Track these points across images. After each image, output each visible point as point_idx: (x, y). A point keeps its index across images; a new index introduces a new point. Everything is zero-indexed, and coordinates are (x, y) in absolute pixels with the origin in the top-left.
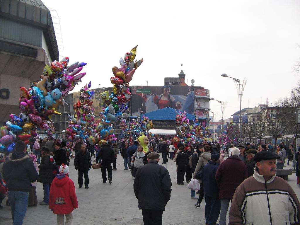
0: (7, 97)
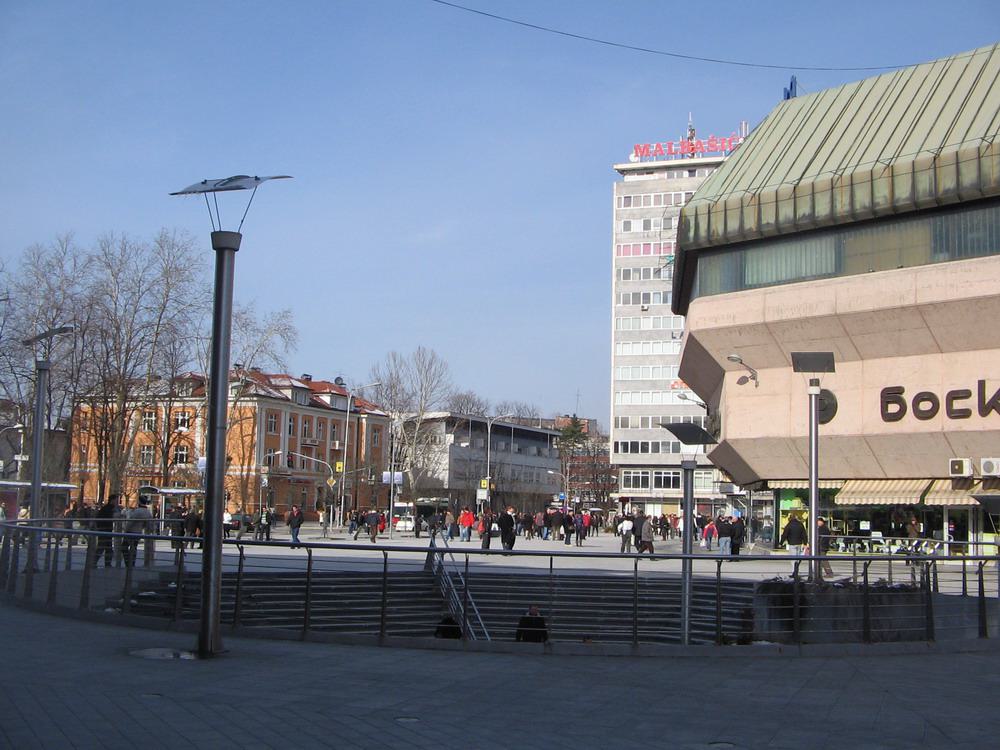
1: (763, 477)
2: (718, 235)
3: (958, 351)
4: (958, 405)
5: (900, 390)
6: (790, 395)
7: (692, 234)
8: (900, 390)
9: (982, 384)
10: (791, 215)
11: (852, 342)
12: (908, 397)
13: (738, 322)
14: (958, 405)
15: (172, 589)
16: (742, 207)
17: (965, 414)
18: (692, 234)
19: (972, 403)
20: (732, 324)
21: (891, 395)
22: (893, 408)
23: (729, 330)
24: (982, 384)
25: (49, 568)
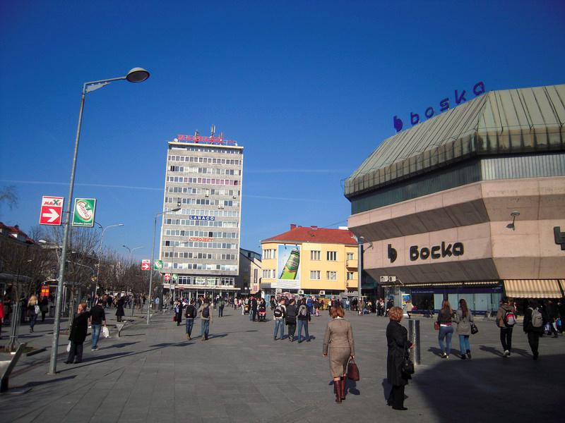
0: (461, 253)
1: (501, 278)
2: (505, 148)
3: (388, 238)
4: (436, 252)
5: (416, 247)
6: (539, 234)
7: (485, 146)
8: (416, 247)
9: (443, 243)
10: (559, 141)
11: (538, 212)
12: (419, 250)
13: (520, 194)
14: (436, 252)
15: (13, 238)
16: (409, 165)
17: (438, 256)
18: (485, 146)
19: (440, 252)
20: (368, 223)
21: (414, 249)
22: (414, 255)
23: (512, 198)
24: (443, 243)
25: (240, 150)
